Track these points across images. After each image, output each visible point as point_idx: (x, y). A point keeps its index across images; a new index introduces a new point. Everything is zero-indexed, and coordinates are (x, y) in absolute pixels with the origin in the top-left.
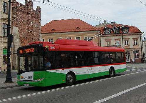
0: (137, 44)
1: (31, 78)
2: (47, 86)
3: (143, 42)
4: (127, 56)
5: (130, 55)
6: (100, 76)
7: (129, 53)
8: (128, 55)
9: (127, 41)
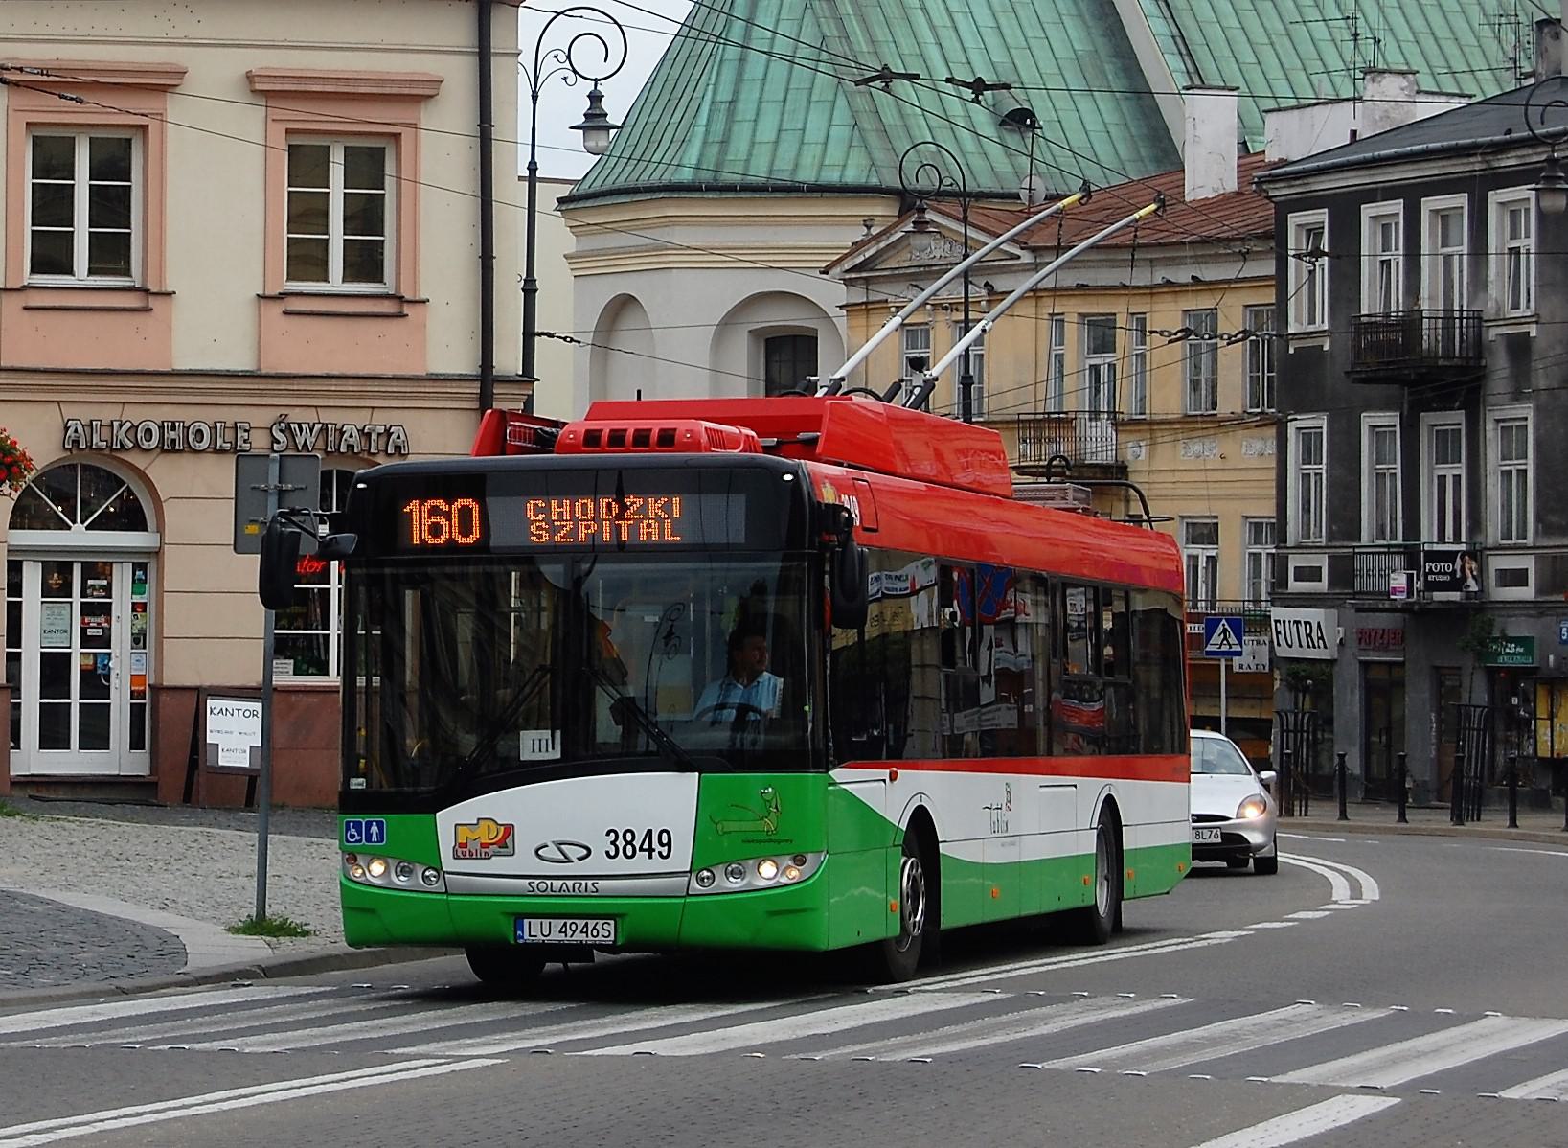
0: (365, 262)
1: (659, 842)
2: (831, 948)
3: (556, 234)
4: (56, 586)
5: (144, 565)
6: (1024, 913)
7: (130, 517)
8: (97, 569)
9: (113, 161)
